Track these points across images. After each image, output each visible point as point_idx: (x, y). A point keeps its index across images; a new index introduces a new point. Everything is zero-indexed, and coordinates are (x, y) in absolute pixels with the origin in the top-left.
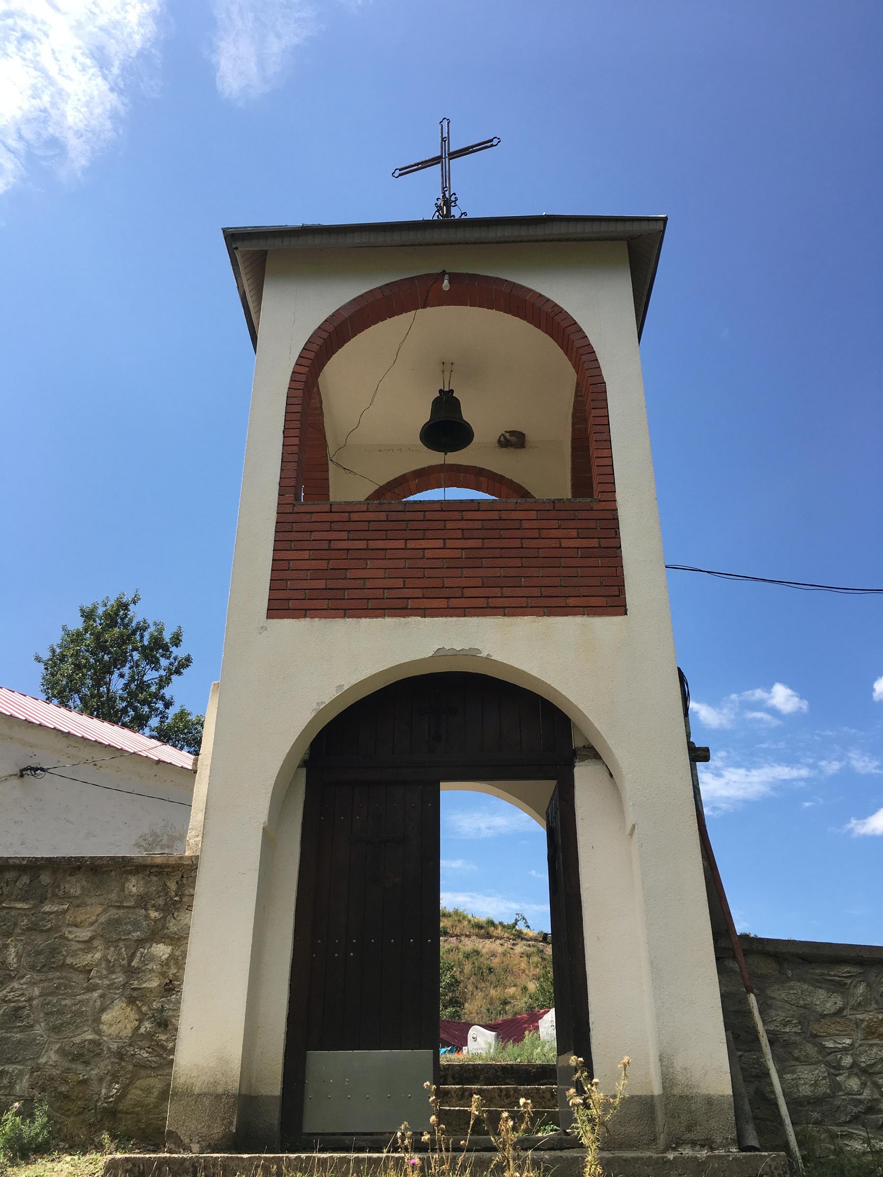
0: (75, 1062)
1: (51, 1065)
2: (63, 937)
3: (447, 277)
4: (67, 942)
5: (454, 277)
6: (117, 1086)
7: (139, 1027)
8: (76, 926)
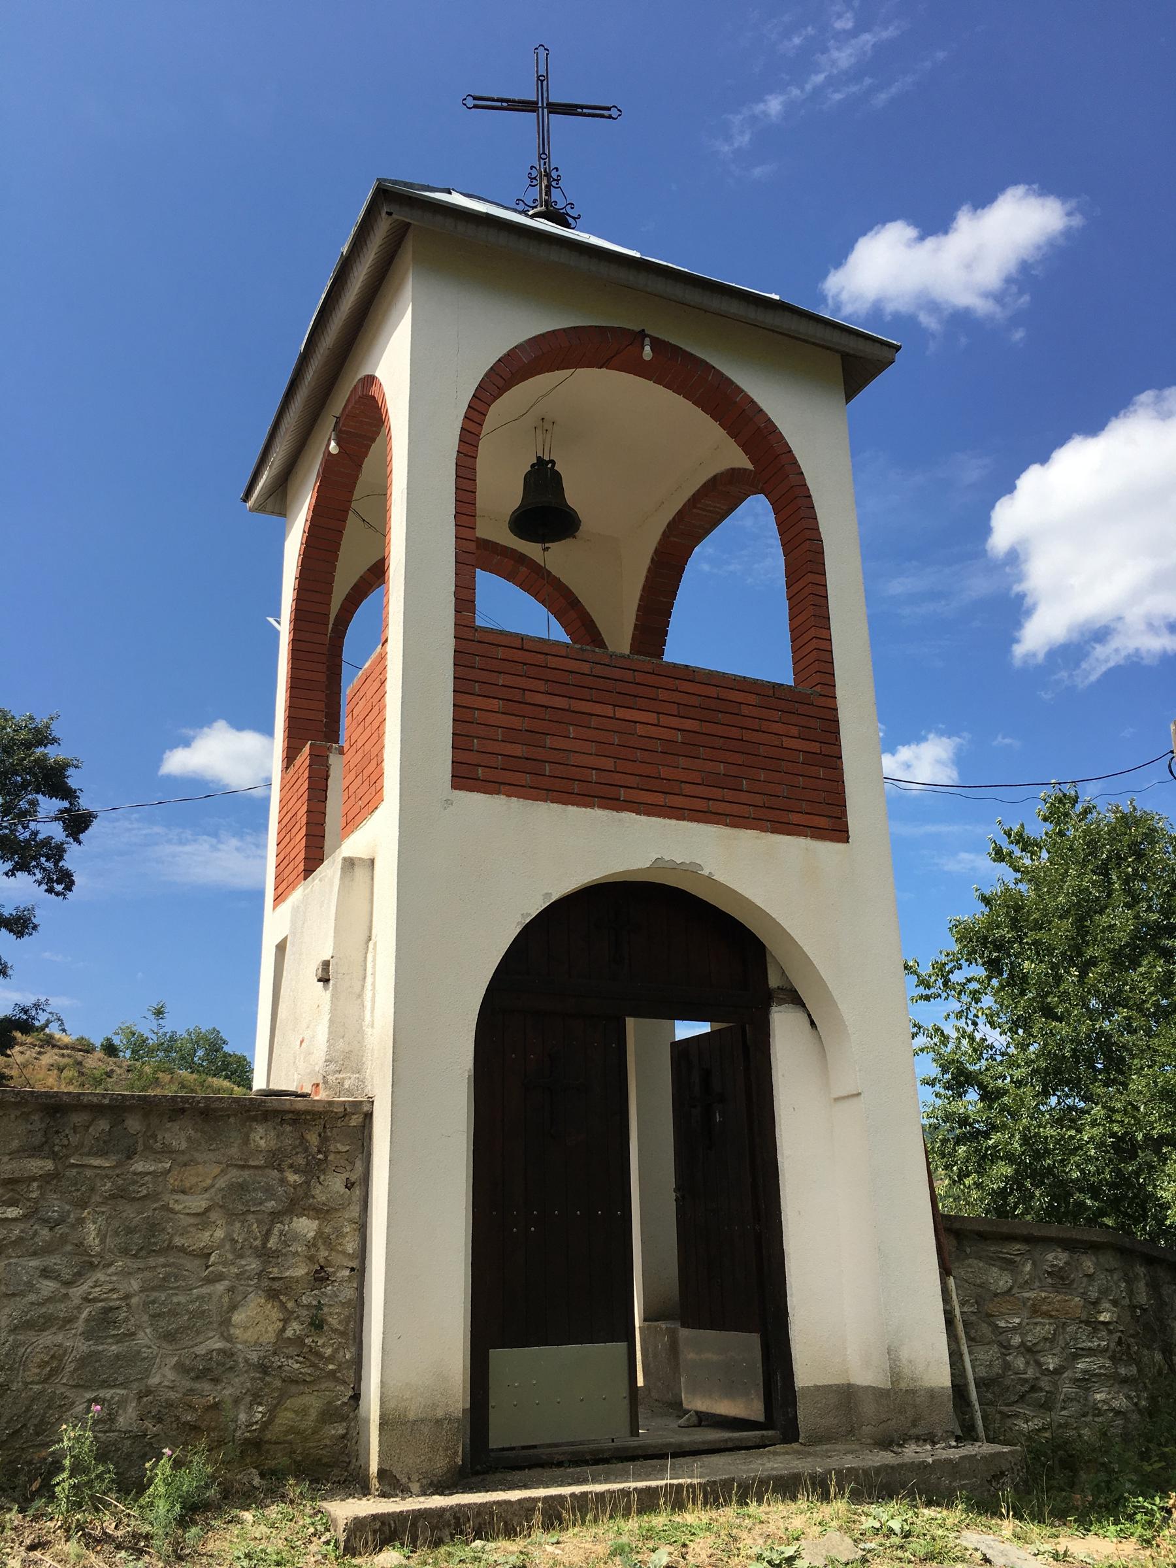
0: (199, 1380)
1: (168, 1387)
2: (166, 1208)
3: (647, 340)
4: (171, 1216)
5: (657, 344)
6: (260, 1409)
7: (283, 1330)
8: (184, 1192)
